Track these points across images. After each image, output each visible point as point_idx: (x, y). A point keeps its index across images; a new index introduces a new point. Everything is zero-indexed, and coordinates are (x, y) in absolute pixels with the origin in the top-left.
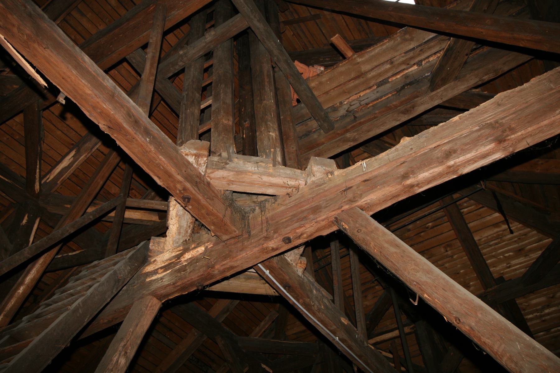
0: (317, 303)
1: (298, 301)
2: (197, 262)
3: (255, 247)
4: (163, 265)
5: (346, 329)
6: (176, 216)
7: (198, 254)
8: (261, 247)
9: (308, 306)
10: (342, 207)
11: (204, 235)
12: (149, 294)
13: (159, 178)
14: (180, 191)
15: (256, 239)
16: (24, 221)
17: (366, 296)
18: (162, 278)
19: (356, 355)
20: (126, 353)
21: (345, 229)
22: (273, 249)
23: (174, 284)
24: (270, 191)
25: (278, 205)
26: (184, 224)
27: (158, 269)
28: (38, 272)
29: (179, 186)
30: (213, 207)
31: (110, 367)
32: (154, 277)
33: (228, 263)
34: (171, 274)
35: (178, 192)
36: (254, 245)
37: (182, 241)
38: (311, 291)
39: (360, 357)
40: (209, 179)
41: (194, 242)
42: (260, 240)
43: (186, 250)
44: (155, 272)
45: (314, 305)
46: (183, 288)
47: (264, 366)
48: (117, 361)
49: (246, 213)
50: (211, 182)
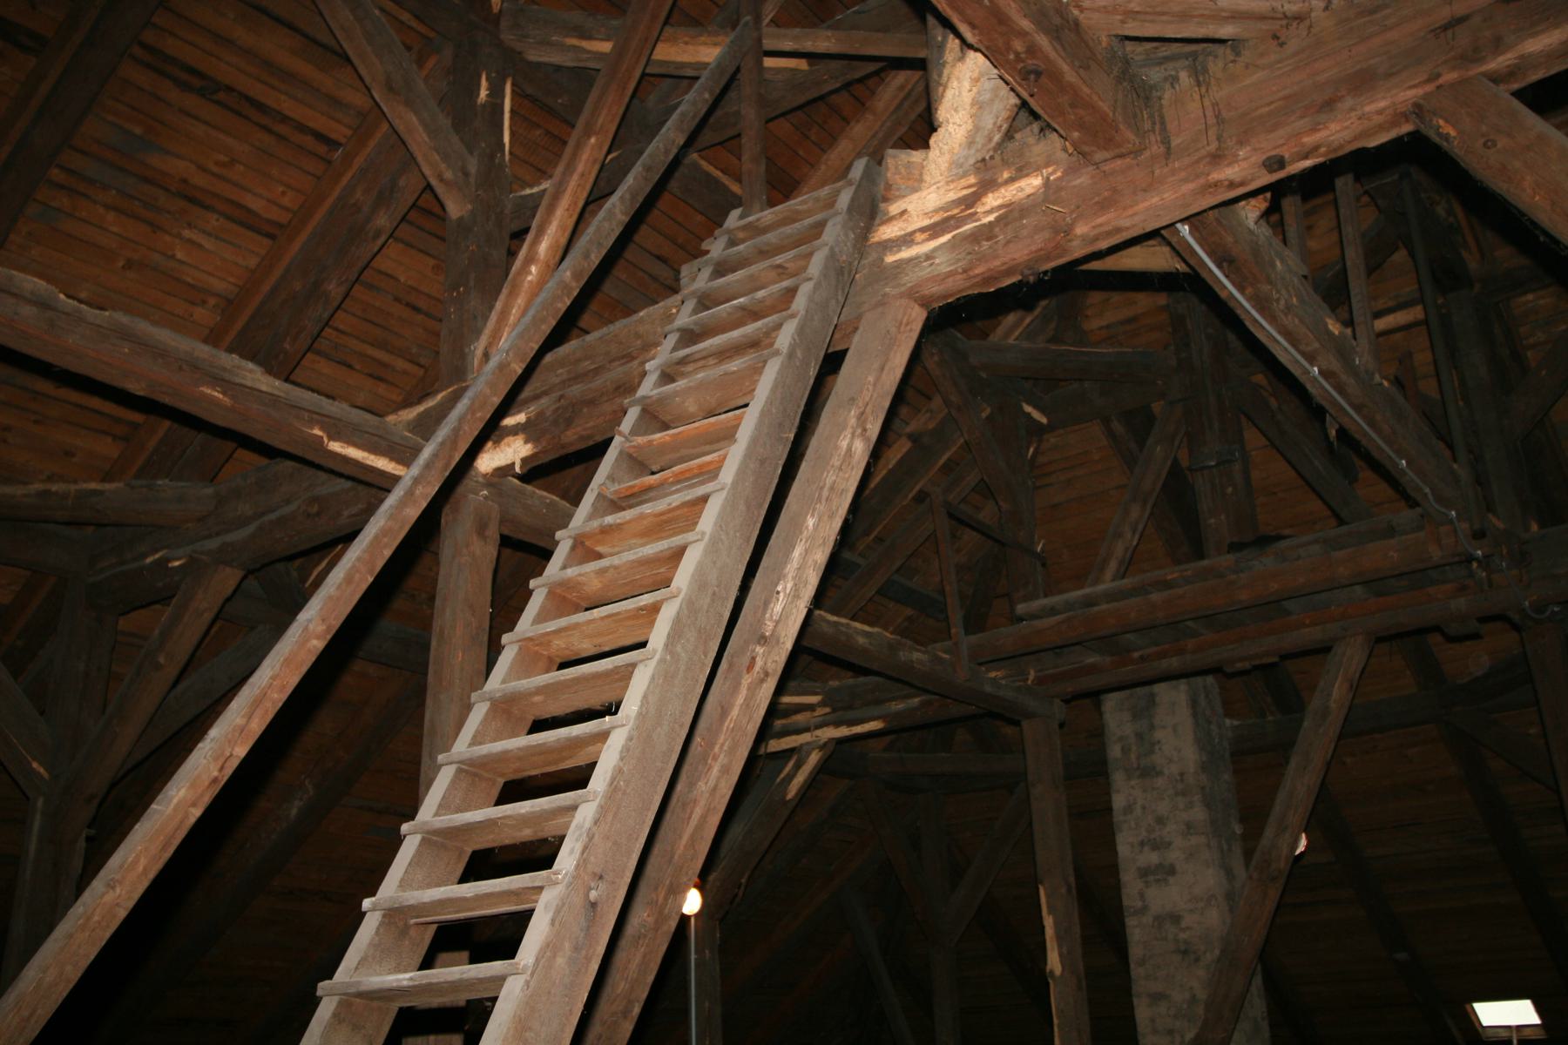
0: (1284, 292)
1: (1241, 289)
2: (1022, 217)
3: (1186, 180)
4: (927, 222)
5: (1343, 352)
6: (972, 105)
7: (1021, 195)
8: (1202, 181)
9: (1262, 304)
10: (1439, 75)
11: (1032, 142)
12: (902, 295)
13: (973, 26)
14: (1017, 54)
15: (1187, 161)
16: (483, 93)
17: (1309, 228)
18: (929, 257)
19: (1351, 405)
20: (865, 430)
21: (1447, 137)
22: (1232, 185)
23: (965, 271)
24: (1226, 31)
25: (1247, 67)
26: (988, 122)
27: (914, 232)
28: (562, 227)
29: (1018, 45)
30: (1091, 88)
31: (836, 462)
32: (906, 254)
33: (1108, 219)
34: (951, 245)
35: (1012, 57)
36: (1183, 174)
37: (972, 161)
38: (1273, 266)
39: (1358, 408)
40: (1076, 12)
41: (1005, 163)
42: (1197, 162)
43: (987, 185)
44: (907, 240)
45: (1278, 300)
46: (987, 280)
47: (1028, 409)
48: (849, 449)
49: (1152, 87)
50: (1082, 17)
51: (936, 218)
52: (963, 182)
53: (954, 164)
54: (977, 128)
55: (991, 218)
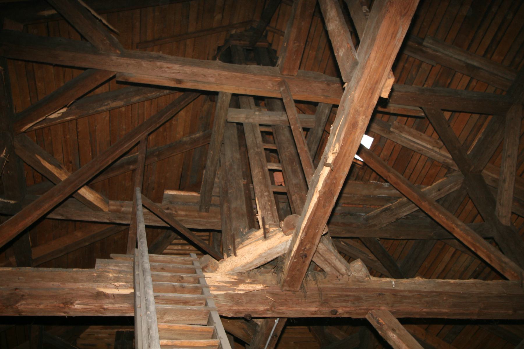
4: (216, 284)
14: (305, 248)
15: (309, 301)
26: (255, 263)
51: (221, 284)
52: (232, 277)
53: (232, 270)
54: (252, 262)
55: (242, 292)
